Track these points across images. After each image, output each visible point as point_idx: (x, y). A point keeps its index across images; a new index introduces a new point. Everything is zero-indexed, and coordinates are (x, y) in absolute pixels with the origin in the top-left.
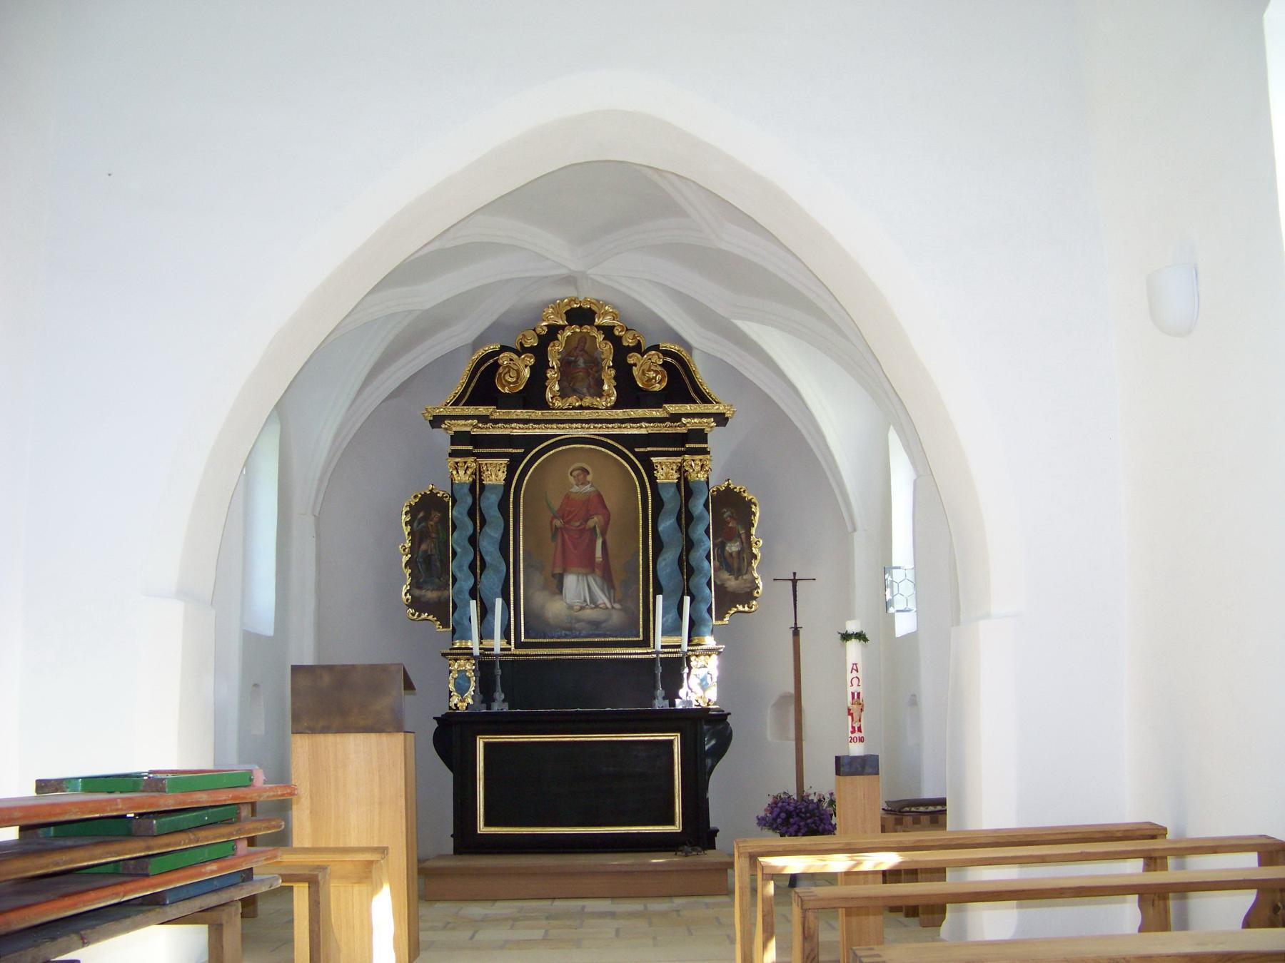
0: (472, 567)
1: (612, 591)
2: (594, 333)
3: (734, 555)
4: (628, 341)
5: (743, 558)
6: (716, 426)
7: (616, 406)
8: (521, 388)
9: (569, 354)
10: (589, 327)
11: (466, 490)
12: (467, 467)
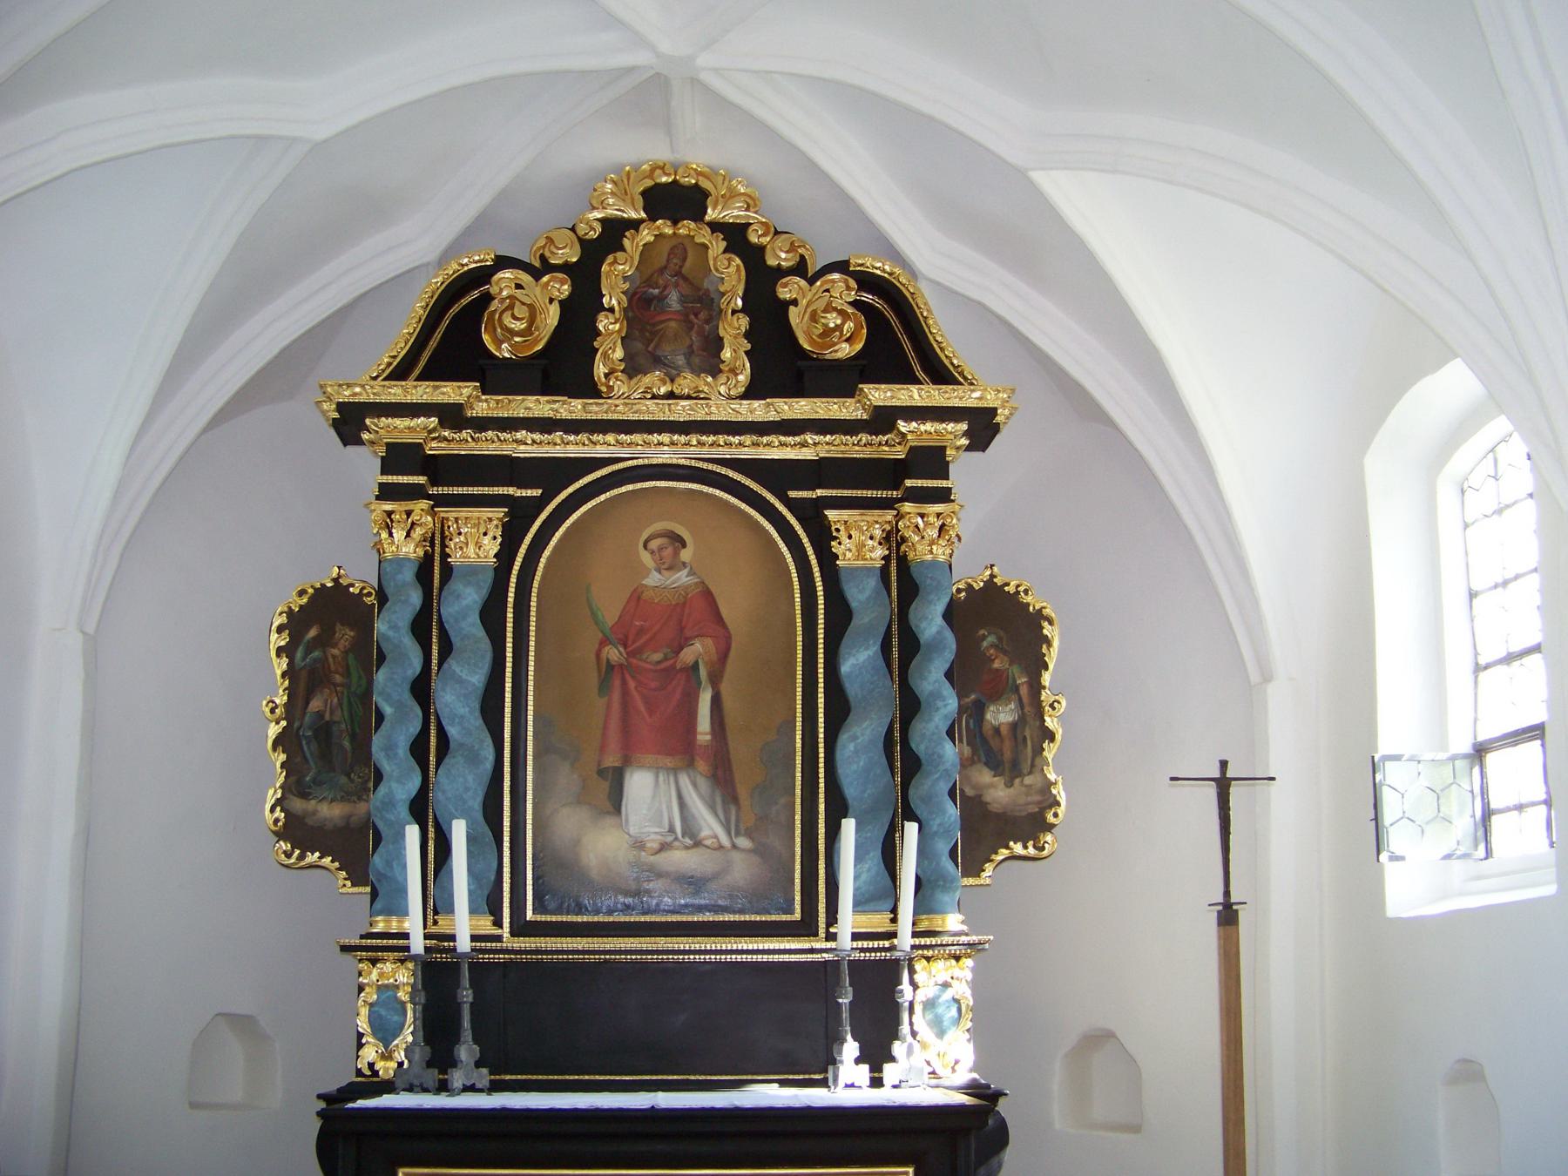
0: (419, 749)
2: (704, 236)
3: (1004, 731)
4: (779, 257)
6: (969, 448)
7: (750, 393)
8: (539, 347)
9: (649, 282)
10: (692, 225)
11: (409, 575)
12: (413, 524)
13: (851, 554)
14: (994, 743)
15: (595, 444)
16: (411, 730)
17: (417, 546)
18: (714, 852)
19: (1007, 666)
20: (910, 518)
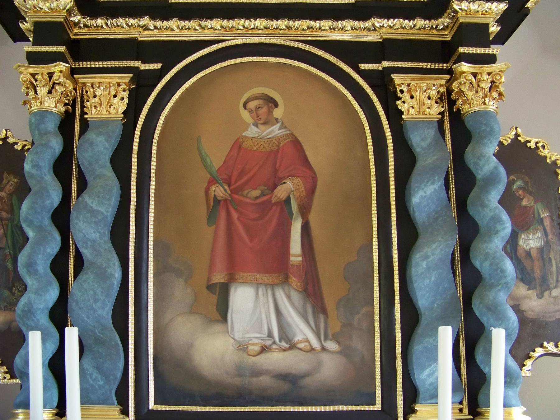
1: (322, 317)
3: (534, 254)
5: (550, 260)
11: (52, 125)
13: (413, 110)
14: (527, 263)
15: (203, 28)
16: (49, 250)
17: (57, 102)
18: (307, 353)
19: (532, 204)
20: (465, 76)
